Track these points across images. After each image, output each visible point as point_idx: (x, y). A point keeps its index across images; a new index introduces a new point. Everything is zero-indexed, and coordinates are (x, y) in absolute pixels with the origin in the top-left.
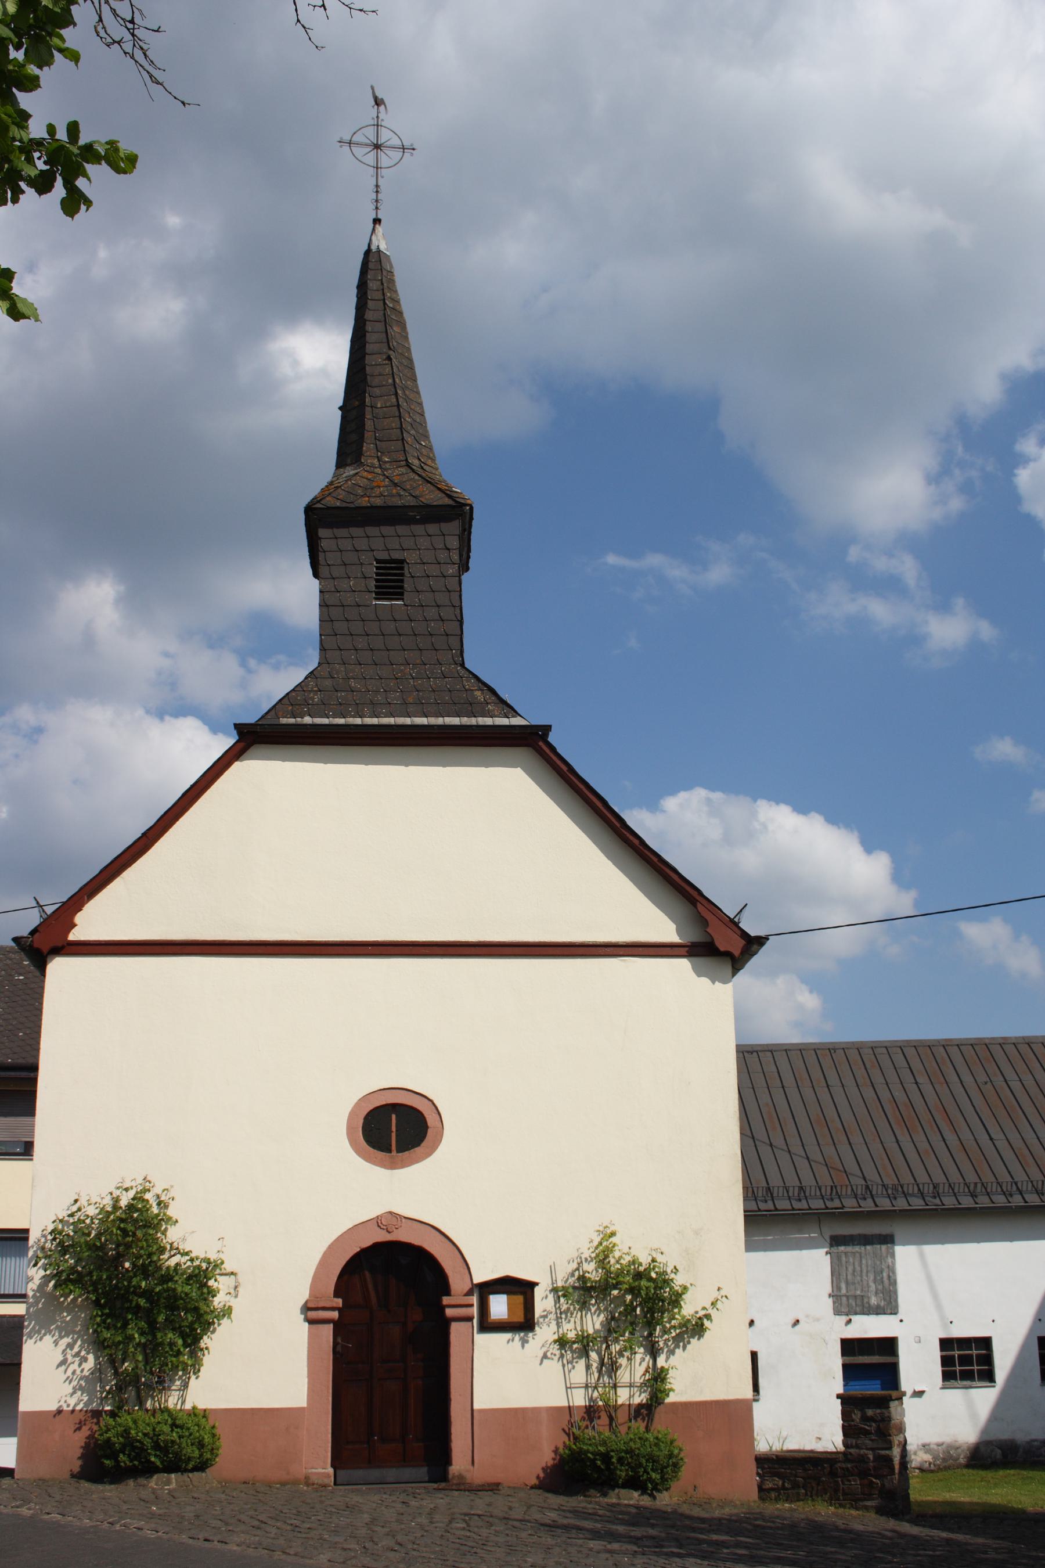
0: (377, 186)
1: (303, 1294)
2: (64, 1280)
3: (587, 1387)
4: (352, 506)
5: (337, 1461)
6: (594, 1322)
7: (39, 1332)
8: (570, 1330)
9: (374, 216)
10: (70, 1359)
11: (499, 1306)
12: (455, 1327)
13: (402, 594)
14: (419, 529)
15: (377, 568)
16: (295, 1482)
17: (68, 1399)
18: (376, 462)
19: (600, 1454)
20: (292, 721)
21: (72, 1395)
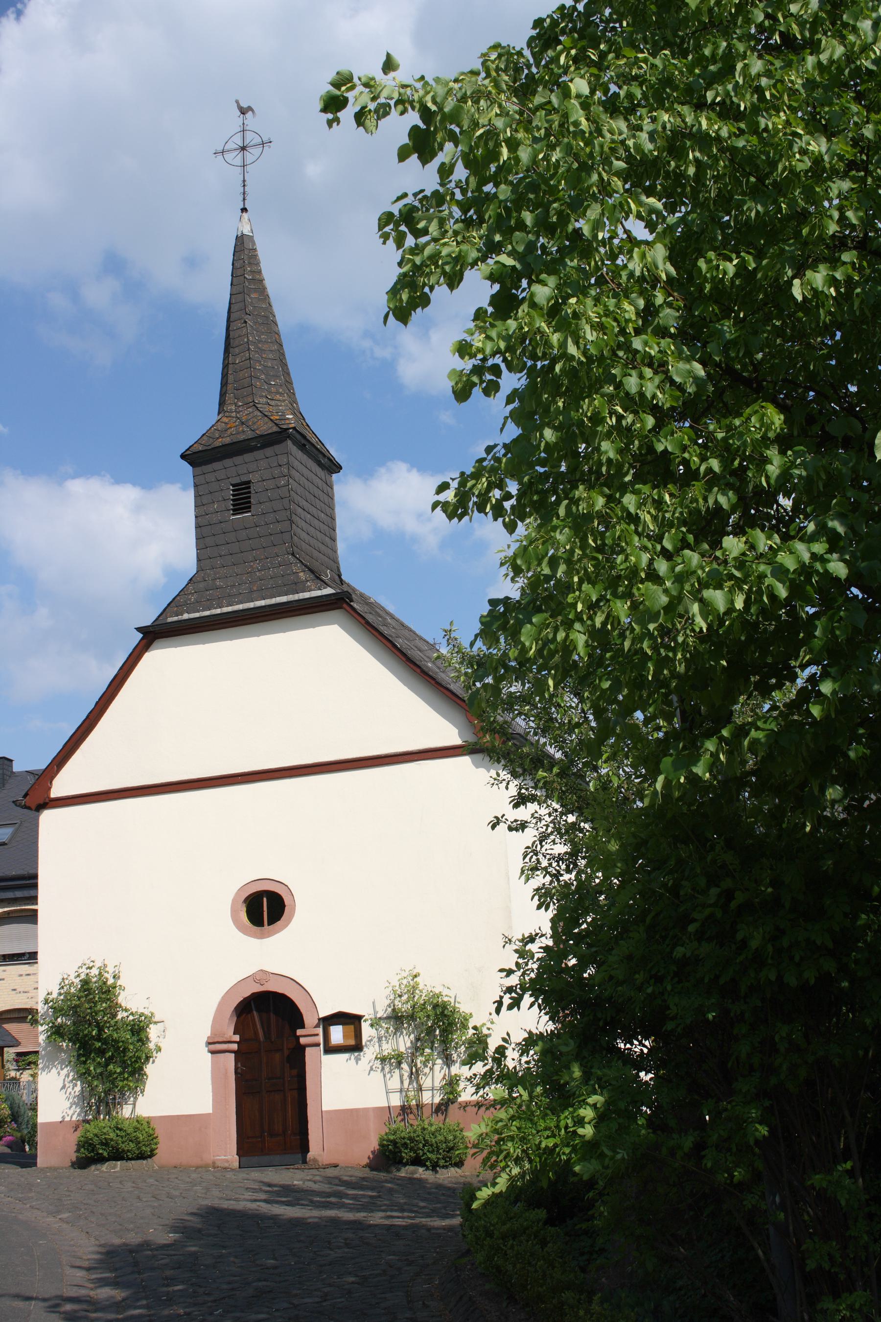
0: (244, 181)
1: (206, 1032)
2: (57, 1032)
3: (401, 1091)
4: (210, 448)
5: (242, 1150)
6: (404, 1042)
7: (48, 1067)
8: (387, 1048)
9: (242, 207)
10: (67, 1085)
11: (337, 1034)
12: (309, 1051)
13: (250, 507)
14: (259, 454)
15: (233, 491)
16: (206, 1166)
17: (68, 1111)
18: (233, 407)
19: (391, 1141)
20: (175, 619)
21: (70, 1108)
